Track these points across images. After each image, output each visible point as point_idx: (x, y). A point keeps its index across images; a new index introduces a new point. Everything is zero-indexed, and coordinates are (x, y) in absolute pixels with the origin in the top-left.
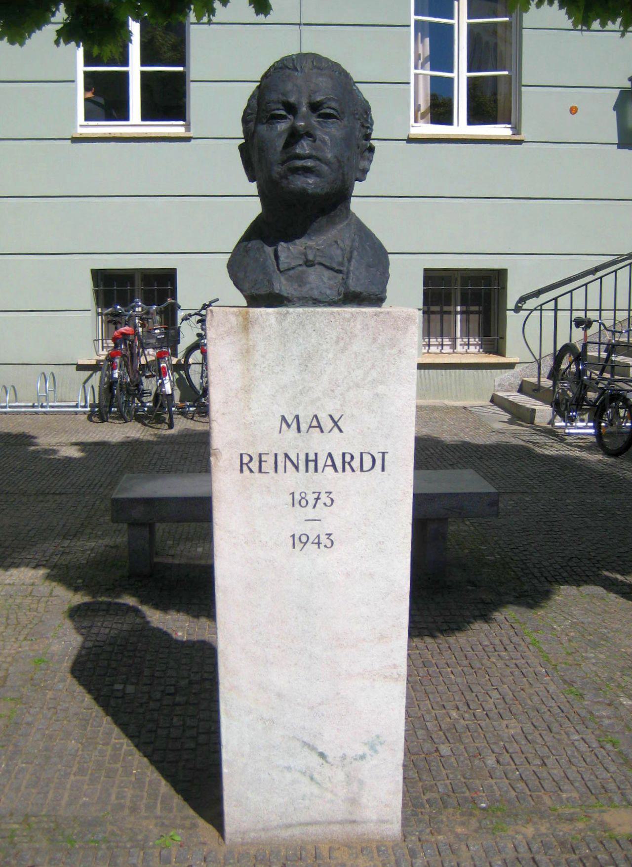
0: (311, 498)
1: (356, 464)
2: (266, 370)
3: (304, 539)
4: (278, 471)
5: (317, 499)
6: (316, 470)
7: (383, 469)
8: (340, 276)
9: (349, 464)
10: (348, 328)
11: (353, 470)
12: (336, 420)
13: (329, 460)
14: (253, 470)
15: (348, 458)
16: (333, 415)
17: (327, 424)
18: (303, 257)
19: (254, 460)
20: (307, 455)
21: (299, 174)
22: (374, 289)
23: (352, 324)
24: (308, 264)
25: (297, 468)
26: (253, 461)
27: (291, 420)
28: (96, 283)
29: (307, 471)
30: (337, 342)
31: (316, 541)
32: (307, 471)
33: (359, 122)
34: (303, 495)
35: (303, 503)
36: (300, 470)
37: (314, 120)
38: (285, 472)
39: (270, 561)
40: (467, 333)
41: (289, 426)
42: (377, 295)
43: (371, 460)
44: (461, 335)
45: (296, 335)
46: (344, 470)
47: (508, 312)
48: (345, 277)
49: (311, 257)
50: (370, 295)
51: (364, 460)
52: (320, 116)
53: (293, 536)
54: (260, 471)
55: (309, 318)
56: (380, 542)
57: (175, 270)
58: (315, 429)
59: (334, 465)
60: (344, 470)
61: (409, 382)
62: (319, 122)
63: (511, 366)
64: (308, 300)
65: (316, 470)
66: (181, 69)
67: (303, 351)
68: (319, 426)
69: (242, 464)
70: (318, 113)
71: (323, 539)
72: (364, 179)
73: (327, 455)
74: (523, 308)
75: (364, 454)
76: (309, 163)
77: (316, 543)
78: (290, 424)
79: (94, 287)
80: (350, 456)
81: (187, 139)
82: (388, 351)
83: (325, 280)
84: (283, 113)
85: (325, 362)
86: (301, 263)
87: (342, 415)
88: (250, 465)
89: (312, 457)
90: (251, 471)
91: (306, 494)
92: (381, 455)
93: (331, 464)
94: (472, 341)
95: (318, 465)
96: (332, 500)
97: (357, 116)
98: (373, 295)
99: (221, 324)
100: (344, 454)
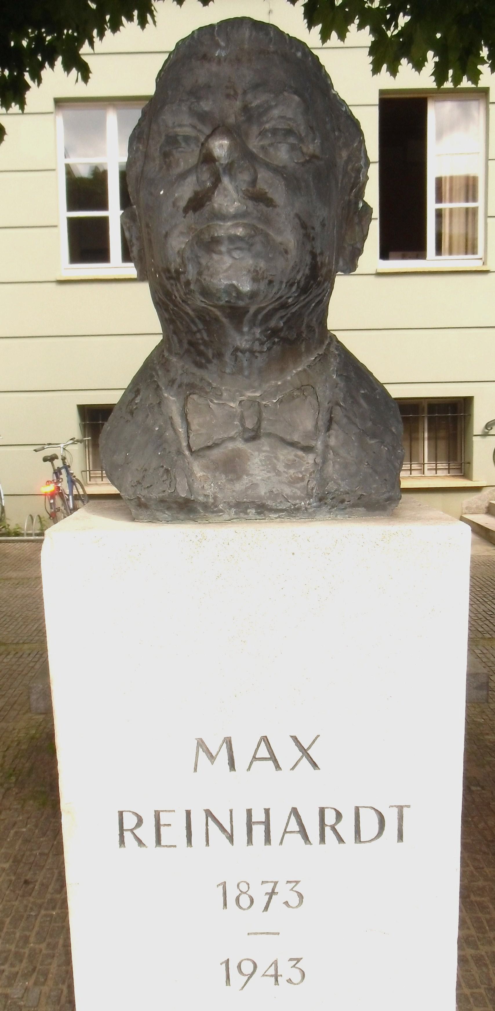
3: (247, 968)
5: (272, 894)
6: (268, 840)
7: (400, 837)
8: (310, 458)
9: (333, 828)
11: (340, 840)
12: (305, 760)
13: (293, 819)
20: (249, 812)
25: (231, 838)
29: (250, 841)
32: (250, 841)
34: (244, 887)
40: (435, 458)
41: (212, 758)
43: (375, 819)
44: (429, 460)
46: (322, 839)
47: (475, 439)
48: (319, 460)
53: (227, 962)
54: (158, 841)
60: (322, 839)
63: (478, 489)
64: (247, 508)
65: (268, 840)
68: (273, 758)
71: (286, 970)
74: (490, 434)
77: (272, 976)
78: (214, 755)
80: (334, 813)
83: (281, 467)
89: (259, 816)
90: (140, 843)
92: (396, 810)
93: (297, 828)
94: (440, 466)
96: (301, 896)
100: (322, 812)
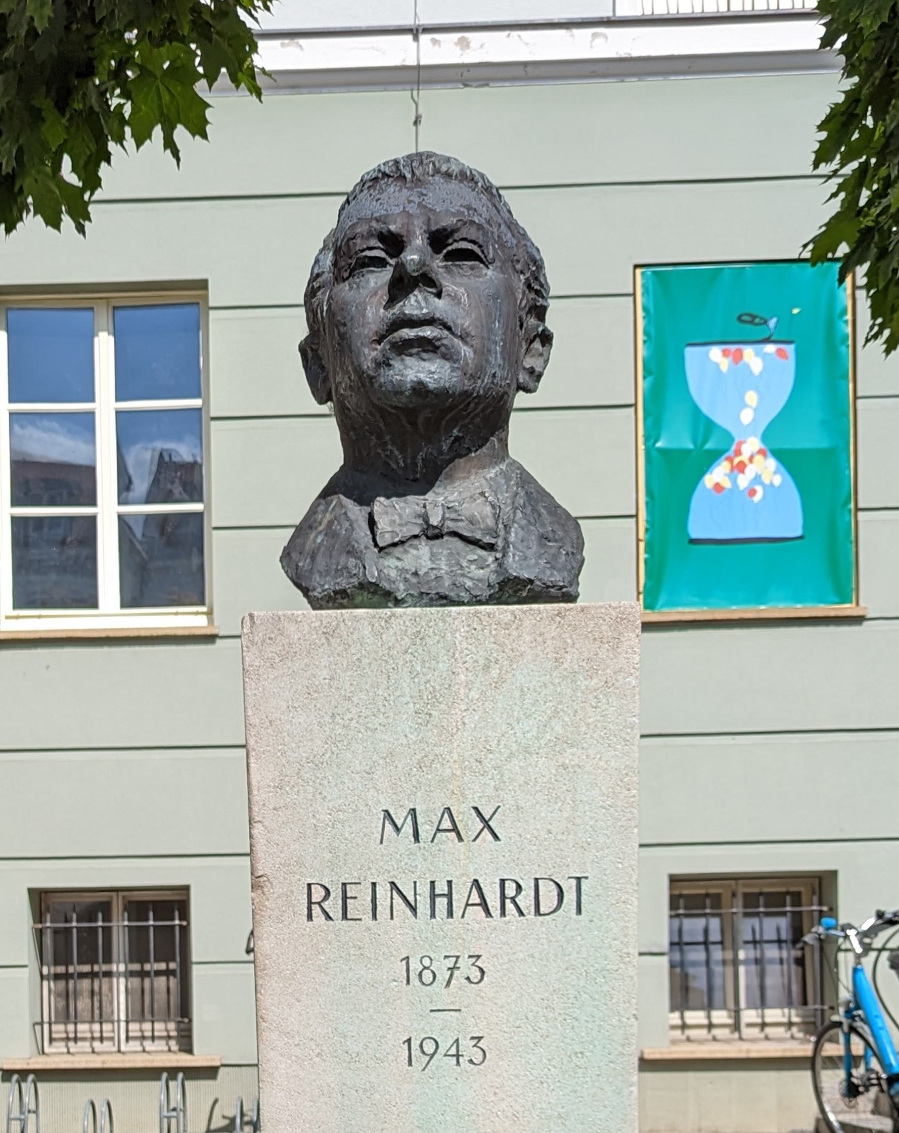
0: (442, 967)
1: (526, 900)
2: (354, 724)
3: (429, 1047)
4: (378, 917)
6: (450, 914)
9: (513, 900)
10: (507, 642)
11: (521, 913)
12: (487, 817)
14: (331, 915)
15: (510, 891)
16: (480, 808)
17: (470, 825)
18: (420, 521)
19: (332, 895)
21: (411, 355)
22: (557, 578)
23: (515, 633)
24: (429, 534)
25: (414, 909)
26: (331, 897)
27: (402, 819)
28: (38, 914)
29: (433, 915)
30: (486, 668)
31: (453, 1051)
33: (522, 277)
34: (426, 962)
35: (427, 976)
36: (418, 914)
37: (437, 264)
38: (392, 918)
39: (365, 1090)
41: (398, 830)
42: (562, 587)
45: (408, 657)
46: (503, 913)
48: (499, 555)
49: (435, 521)
50: (548, 587)
51: (541, 893)
52: (449, 257)
54: (345, 916)
55: (432, 623)
56: (576, 1053)
57: (186, 889)
58: (448, 834)
59: (484, 904)
60: (503, 913)
61: (624, 740)
62: (446, 267)
65: (450, 914)
66: (197, 403)
67: (422, 687)
68: (455, 829)
69: (310, 903)
70: (445, 251)
71: (466, 1045)
72: (535, 391)
73: (470, 885)
75: (540, 882)
76: (428, 332)
77: (453, 1056)
78: (399, 826)
79: (35, 922)
81: (210, 639)
82: (583, 683)
84: (382, 254)
85: (463, 707)
86: (416, 533)
87: (499, 807)
88: (326, 905)
90: (328, 917)
91: (431, 959)
92: (574, 882)
93: (478, 901)
95: (454, 903)
96: (482, 972)
97: (519, 267)
98: (553, 587)
99: (270, 639)
